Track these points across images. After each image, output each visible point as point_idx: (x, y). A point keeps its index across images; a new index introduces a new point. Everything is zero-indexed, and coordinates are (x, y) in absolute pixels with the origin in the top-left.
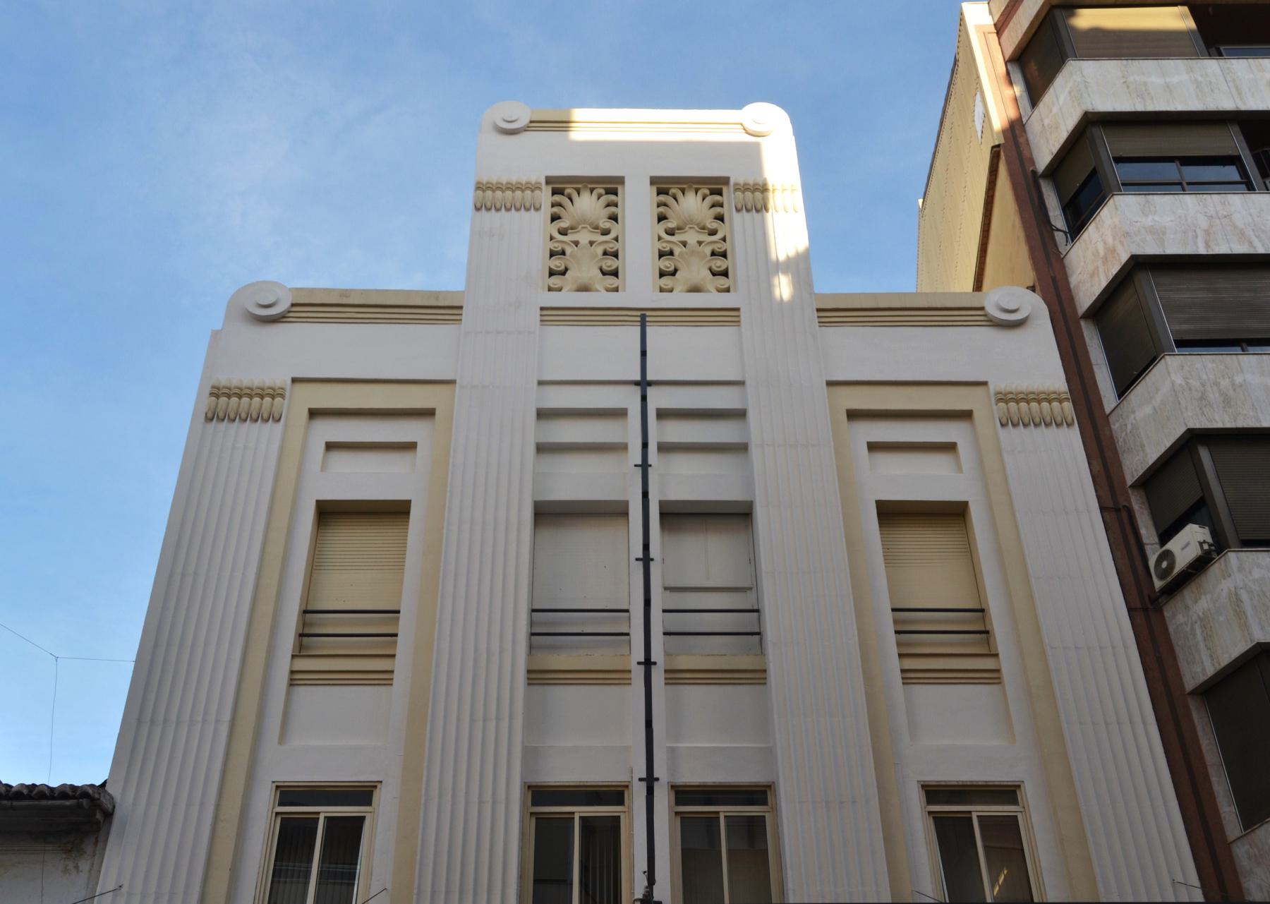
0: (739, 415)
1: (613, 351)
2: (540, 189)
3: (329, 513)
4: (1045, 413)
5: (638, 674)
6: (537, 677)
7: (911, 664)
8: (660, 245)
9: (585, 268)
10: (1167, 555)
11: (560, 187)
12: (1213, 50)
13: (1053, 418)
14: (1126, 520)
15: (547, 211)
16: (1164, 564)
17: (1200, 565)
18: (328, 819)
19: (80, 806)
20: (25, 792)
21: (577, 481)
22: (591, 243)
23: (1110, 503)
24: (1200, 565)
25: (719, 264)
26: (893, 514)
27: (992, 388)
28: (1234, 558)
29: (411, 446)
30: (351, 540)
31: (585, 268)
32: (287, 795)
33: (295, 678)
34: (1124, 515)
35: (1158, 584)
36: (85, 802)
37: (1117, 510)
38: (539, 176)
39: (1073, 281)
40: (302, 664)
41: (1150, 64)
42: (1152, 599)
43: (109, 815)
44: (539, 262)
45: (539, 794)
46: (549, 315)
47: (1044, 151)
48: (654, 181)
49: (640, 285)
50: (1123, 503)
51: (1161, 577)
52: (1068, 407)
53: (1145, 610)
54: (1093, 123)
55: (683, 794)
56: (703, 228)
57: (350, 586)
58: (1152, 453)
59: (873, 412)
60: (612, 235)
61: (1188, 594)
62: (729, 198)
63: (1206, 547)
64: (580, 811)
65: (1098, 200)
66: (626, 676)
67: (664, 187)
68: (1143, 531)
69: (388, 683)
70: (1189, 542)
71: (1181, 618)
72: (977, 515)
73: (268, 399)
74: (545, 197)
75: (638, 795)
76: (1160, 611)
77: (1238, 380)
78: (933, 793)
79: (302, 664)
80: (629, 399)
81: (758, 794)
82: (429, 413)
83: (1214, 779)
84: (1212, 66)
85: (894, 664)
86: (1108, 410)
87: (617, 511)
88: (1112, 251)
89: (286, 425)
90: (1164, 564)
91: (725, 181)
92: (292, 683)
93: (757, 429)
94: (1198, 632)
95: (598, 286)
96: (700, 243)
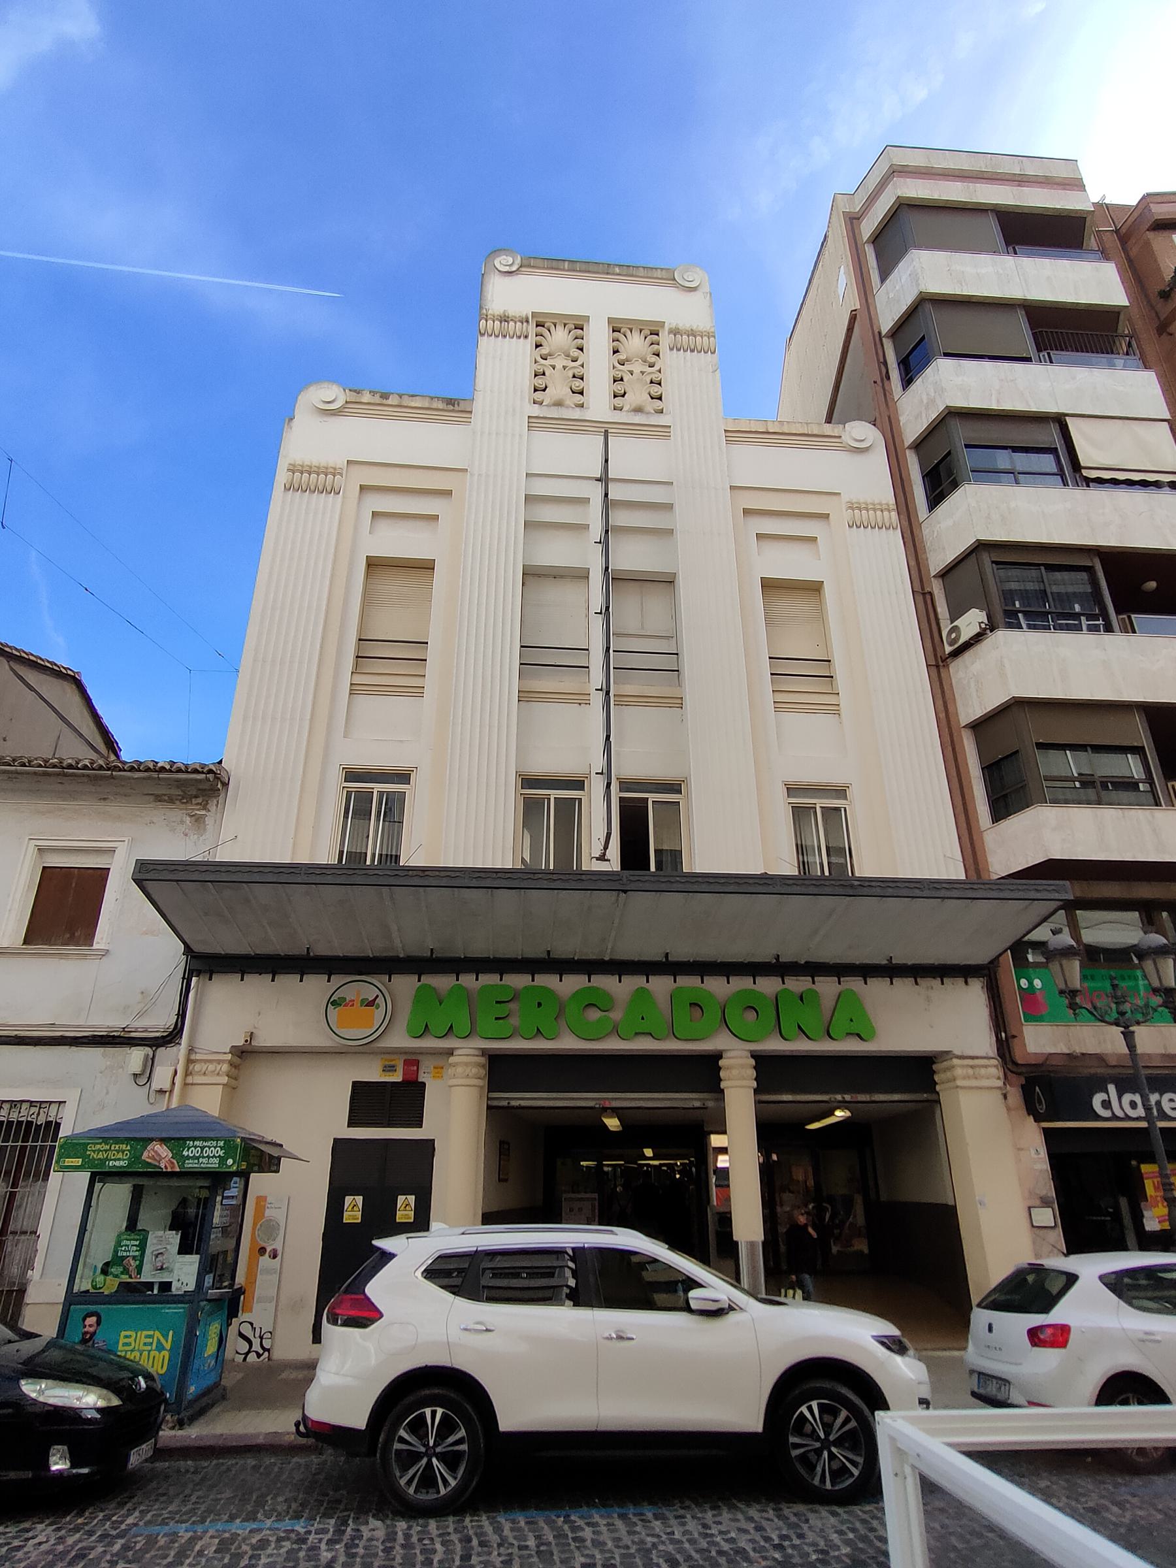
0: (669, 507)
1: (583, 454)
2: (527, 322)
3: (374, 565)
4: (886, 520)
5: (598, 699)
6: (524, 696)
7: (781, 697)
8: (613, 373)
9: (558, 388)
10: (955, 629)
11: (541, 322)
12: (1011, 249)
13: (869, 522)
14: (929, 602)
15: (532, 339)
16: (953, 635)
17: (978, 638)
18: (381, 794)
19: (208, 780)
20: (168, 767)
21: (555, 552)
22: (564, 368)
23: (918, 588)
24: (978, 638)
25: (577, 384)
26: (769, 586)
27: (845, 498)
28: (1002, 636)
29: (435, 518)
30: (392, 585)
31: (558, 388)
32: (352, 775)
33: (354, 690)
34: (928, 597)
35: (948, 649)
36: (211, 776)
37: (924, 594)
38: (526, 310)
39: (903, 419)
40: (359, 679)
41: (967, 257)
42: (942, 657)
43: (226, 785)
44: (526, 381)
45: (529, 782)
46: (534, 422)
47: (887, 321)
48: (610, 320)
49: (599, 404)
50: (927, 589)
51: (951, 645)
52: (894, 514)
53: (937, 666)
54: (925, 302)
55: (625, 785)
56: (568, 356)
57: (392, 623)
58: (950, 556)
59: (759, 512)
60: (579, 363)
61: (968, 656)
62: (665, 339)
63: (983, 626)
64: (554, 794)
65: (925, 362)
66: (586, 697)
67: (617, 328)
68: (939, 610)
69: (421, 695)
70: (971, 621)
71: (961, 674)
72: (828, 589)
73: (330, 477)
74: (532, 329)
75: (596, 786)
76: (947, 666)
77: (1013, 505)
78: (792, 790)
79: (359, 679)
80: (595, 493)
81: (674, 787)
82: (448, 493)
83: (975, 787)
84: (1009, 261)
85: (770, 698)
86: (921, 520)
87: (582, 575)
88: (932, 401)
89: (344, 497)
90: (953, 635)
92: (352, 693)
93: (680, 520)
94: (973, 685)
95: (568, 402)
96: (643, 373)
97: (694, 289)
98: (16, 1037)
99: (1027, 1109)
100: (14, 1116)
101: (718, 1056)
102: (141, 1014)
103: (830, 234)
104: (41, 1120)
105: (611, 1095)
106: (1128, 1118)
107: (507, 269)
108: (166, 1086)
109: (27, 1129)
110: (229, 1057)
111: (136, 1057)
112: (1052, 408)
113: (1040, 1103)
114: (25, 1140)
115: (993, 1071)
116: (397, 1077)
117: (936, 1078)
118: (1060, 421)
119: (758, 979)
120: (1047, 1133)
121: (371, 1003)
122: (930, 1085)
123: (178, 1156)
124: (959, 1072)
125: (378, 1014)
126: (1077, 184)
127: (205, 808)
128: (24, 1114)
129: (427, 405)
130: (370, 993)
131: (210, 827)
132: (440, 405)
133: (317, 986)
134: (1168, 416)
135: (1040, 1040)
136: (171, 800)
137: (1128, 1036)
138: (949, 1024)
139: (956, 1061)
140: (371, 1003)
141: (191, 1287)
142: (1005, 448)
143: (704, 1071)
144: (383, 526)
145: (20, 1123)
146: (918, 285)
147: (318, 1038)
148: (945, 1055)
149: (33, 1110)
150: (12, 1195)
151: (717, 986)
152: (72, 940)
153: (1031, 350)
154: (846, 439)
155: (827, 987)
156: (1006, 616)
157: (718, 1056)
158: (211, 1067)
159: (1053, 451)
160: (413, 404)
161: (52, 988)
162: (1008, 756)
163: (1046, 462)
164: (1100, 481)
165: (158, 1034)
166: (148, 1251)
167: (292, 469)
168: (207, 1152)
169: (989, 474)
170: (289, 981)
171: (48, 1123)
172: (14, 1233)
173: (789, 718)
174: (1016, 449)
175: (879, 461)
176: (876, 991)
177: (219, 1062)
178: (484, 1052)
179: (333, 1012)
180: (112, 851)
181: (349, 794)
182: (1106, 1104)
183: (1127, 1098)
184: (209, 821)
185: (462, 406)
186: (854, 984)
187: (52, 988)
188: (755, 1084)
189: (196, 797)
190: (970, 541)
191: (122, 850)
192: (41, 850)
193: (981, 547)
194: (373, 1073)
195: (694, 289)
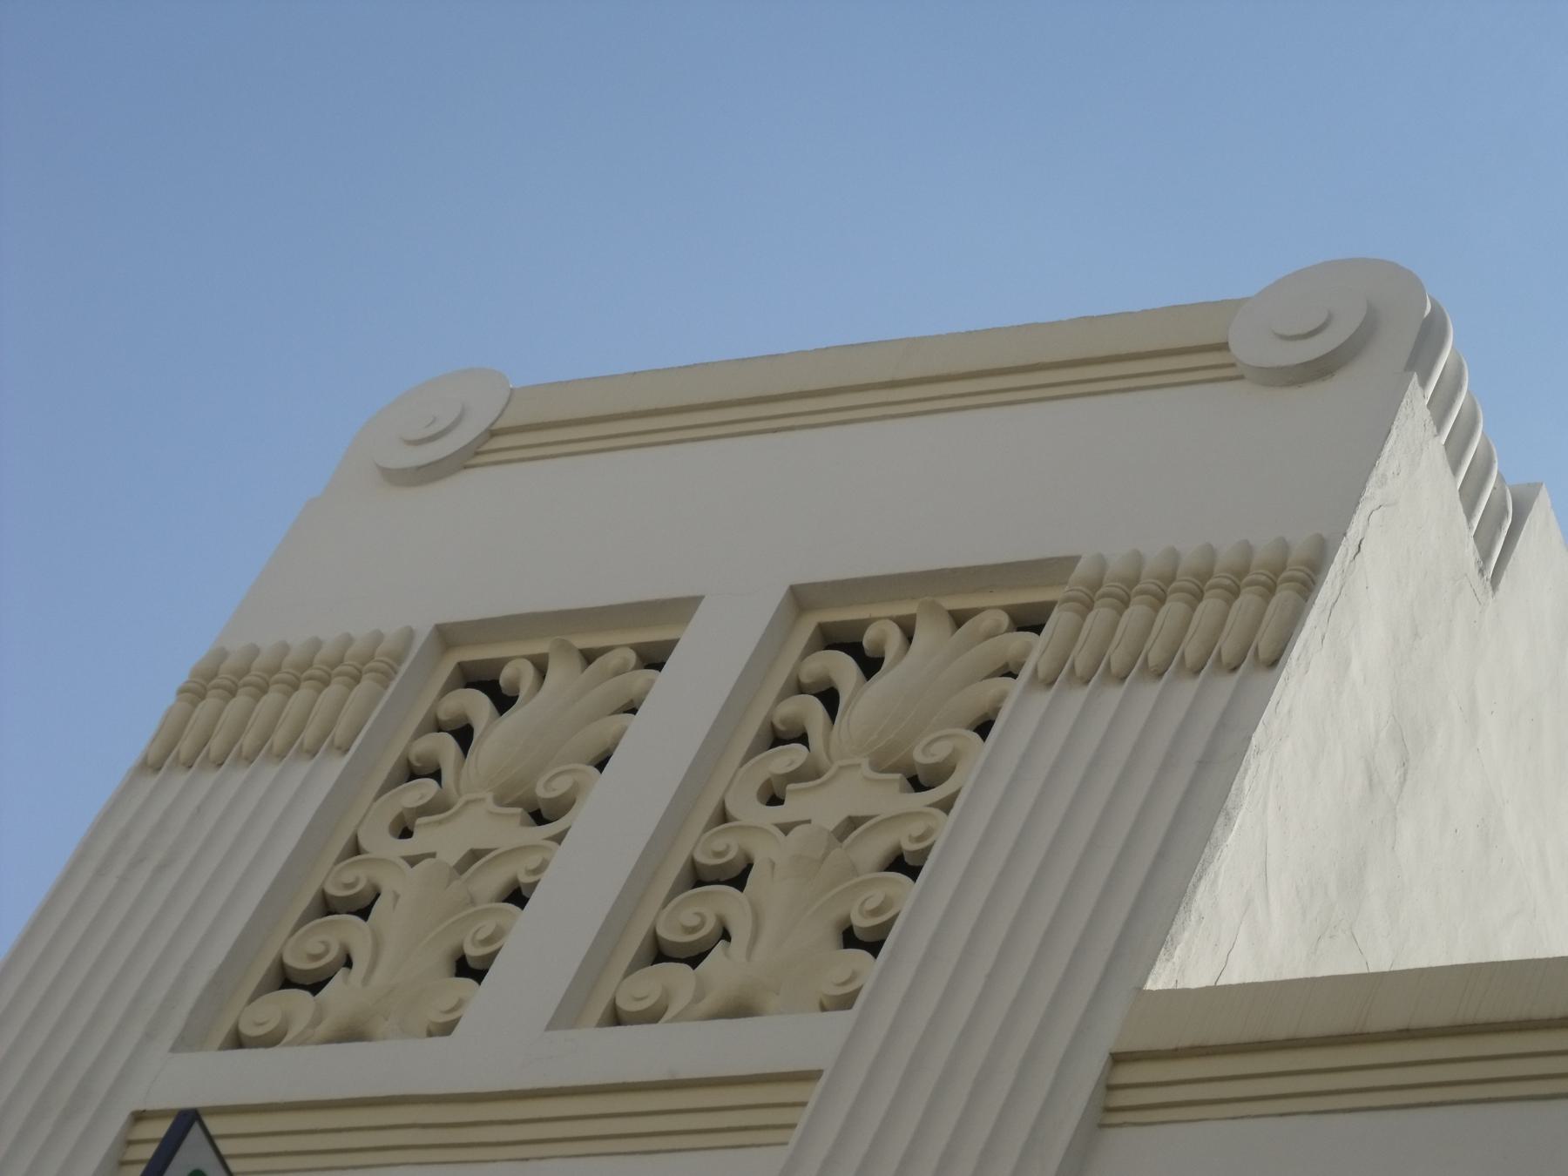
91: (1055, 568)
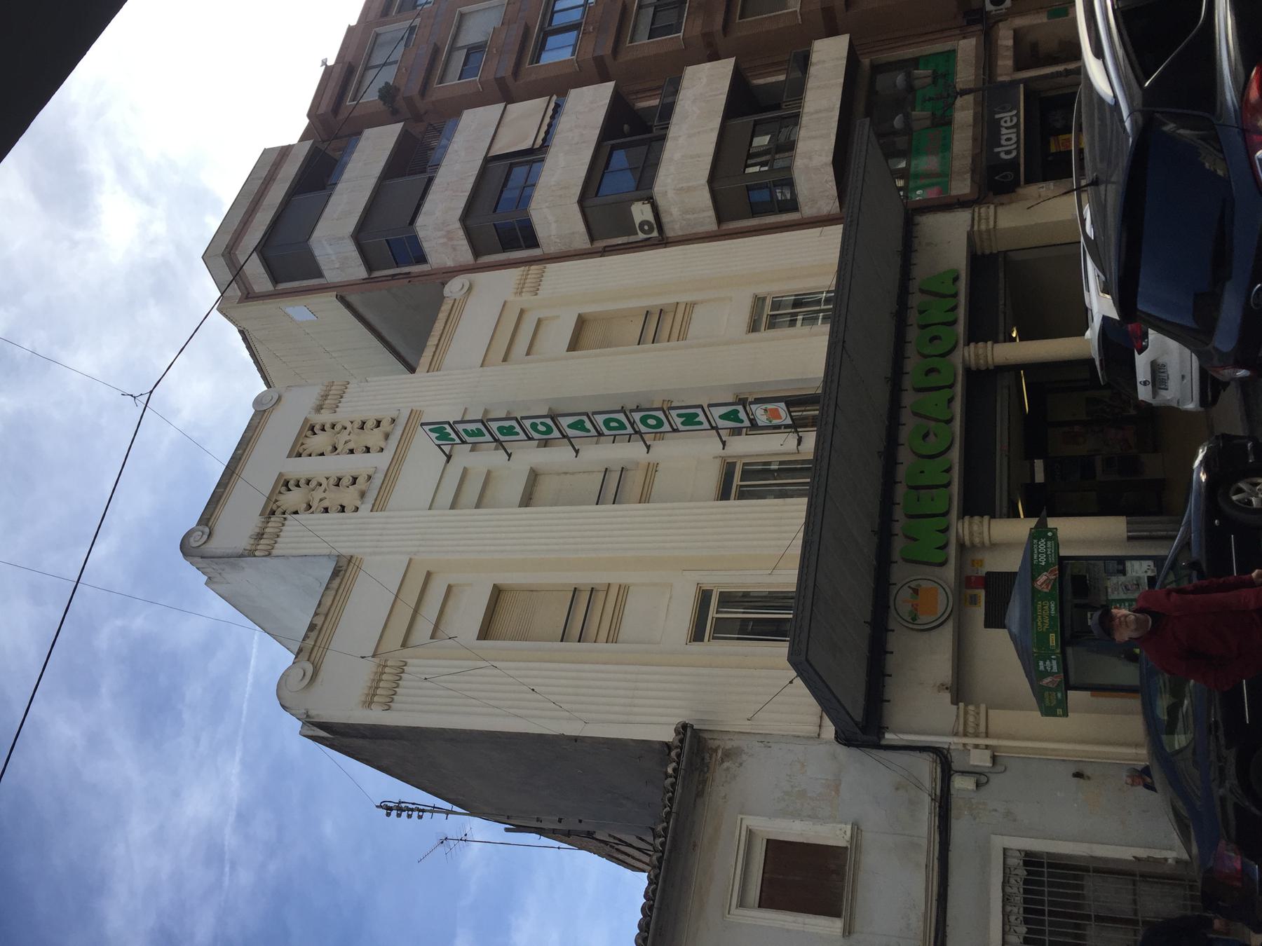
28: (658, 188)
42: (659, 236)
54: (359, 236)
58: (581, 227)
61: (665, 219)
67: (297, 452)
70: (641, 212)
97: (279, 399)
98: (939, 859)
99: (1008, 192)
100: (1019, 899)
101: (968, 371)
102: (919, 786)
103: (245, 325)
104: (1022, 872)
105: (998, 447)
106: (1018, 142)
107: (205, 537)
108: (988, 753)
109: (1029, 884)
110: (961, 705)
111: (961, 784)
112: (479, 163)
113: (1006, 176)
114: (1042, 913)
115: (983, 210)
116: (982, 594)
117: (987, 252)
118: (488, 160)
119: (908, 339)
120: (1029, 181)
121: (916, 591)
122: (993, 257)
123: (1045, 569)
124: (983, 227)
125: (924, 584)
126: (285, 151)
127: (716, 750)
128: (1017, 889)
129: (333, 592)
130: (906, 593)
131: (735, 744)
132: (337, 581)
133: (898, 641)
134: (502, 105)
135: (962, 186)
136: (704, 782)
137: (964, 92)
138: (949, 237)
139: (976, 228)
140: (916, 591)
141: (1151, 563)
142: (502, 192)
143: (981, 381)
144: (449, 627)
145: (1026, 892)
146: (343, 238)
147: (945, 638)
148: (970, 236)
149: (1012, 881)
150: (1099, 918)
151: (913, 364)
152: (840, 872)
153: (425, 176)
154: (458, 296)
155: (915, 300)
156: (644, 185)
157: (968, 371)
158: (971, 719)
159: (511, 166)
160: (329, 603)
161: (891, 890)
162: (749, 196)
163: (520, 172)
164: (544, 140)
165: (939, 770)
166: (1124, 597)
167: (368, 703)
168: (1042, 549)
169: (524, 199)
170: (891, 662)
171: (1026, 863)
172: (1135, 912)
173: (693, 330)
174: (505, 185)
175: (481, 278)
176: (921, 272)
177: (966, 713)
178: (961, 516)
179: (923, 618)
180: (750, 833)
181: (714, 638)
182: (1008, 152)
183: (1003, 142)
184: (729, 745)
185: (344, 562)
186: (914, 286)
187: (891, 890)
188: (986, 518)
189: (703, 759)
190: (576, 207)
191: (752, 821)
192: (742, 904)
193: (581, 202)
194: (979, 612)
195: (279, 399)
